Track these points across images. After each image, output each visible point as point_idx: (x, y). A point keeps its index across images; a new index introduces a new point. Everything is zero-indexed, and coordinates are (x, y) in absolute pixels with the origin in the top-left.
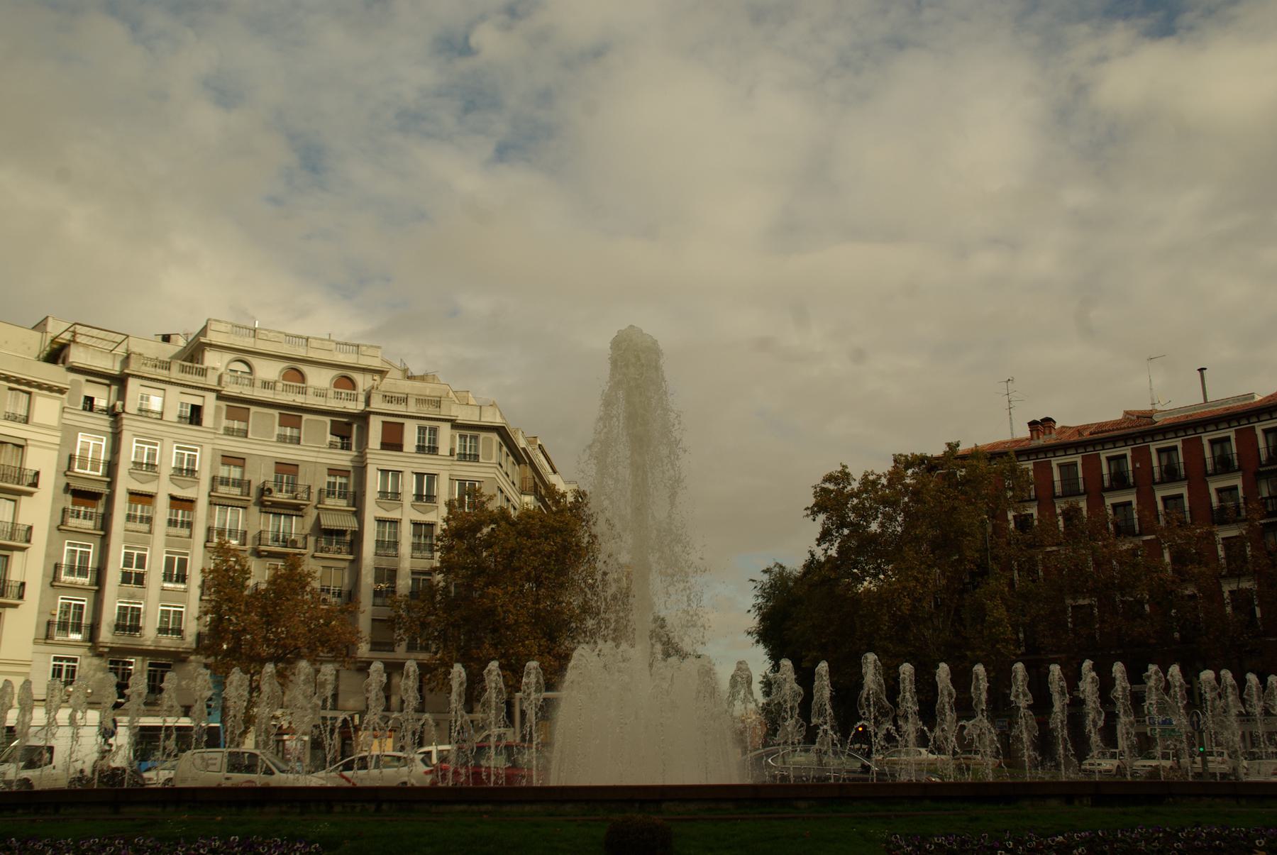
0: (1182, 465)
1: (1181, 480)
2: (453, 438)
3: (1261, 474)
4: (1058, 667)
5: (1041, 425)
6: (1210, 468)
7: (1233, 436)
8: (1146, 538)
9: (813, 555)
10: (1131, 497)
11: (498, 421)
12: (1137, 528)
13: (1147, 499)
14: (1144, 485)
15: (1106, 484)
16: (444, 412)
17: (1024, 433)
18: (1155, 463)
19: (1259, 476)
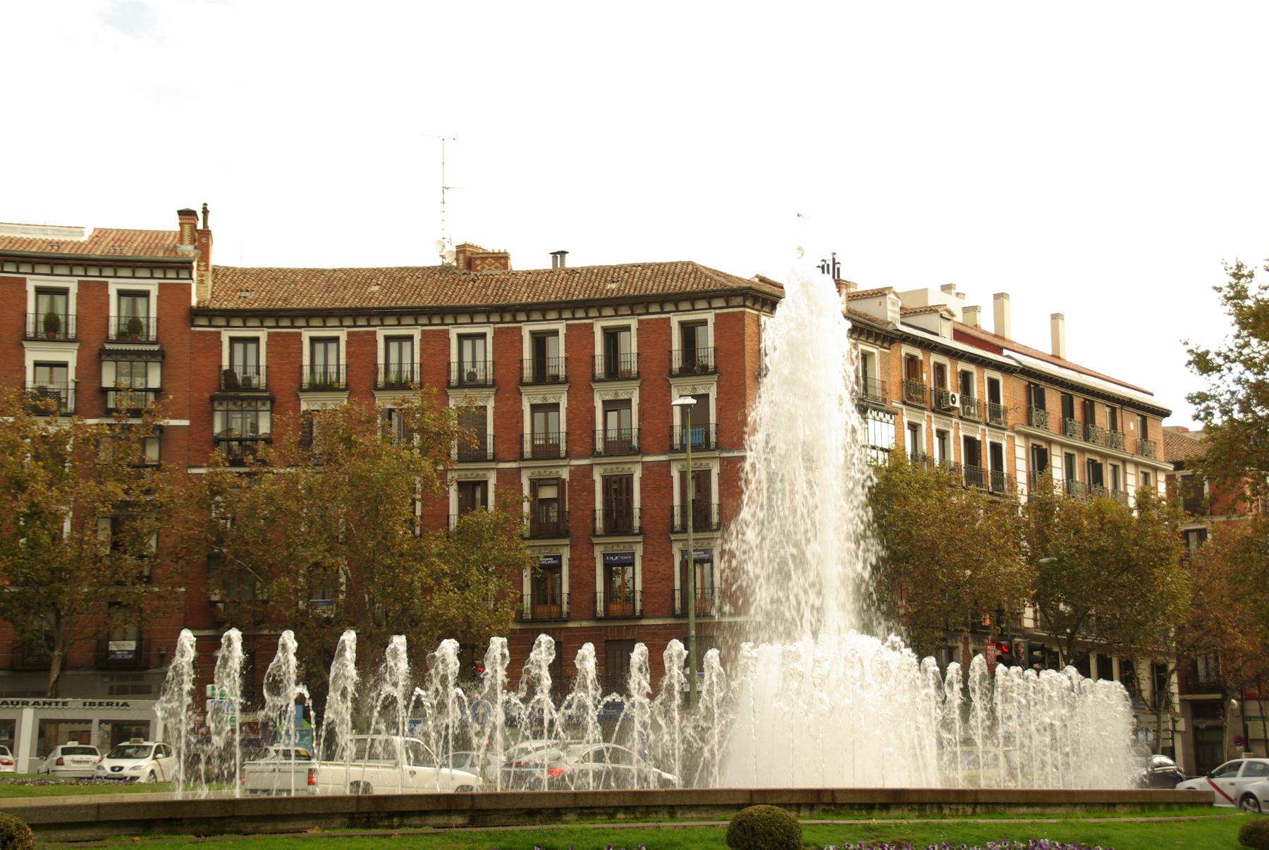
1: (67, 340)
3: (110, 353)
4: (292, 634)
5: (470, 258)
12: (563, 447)
18: (113, 311)
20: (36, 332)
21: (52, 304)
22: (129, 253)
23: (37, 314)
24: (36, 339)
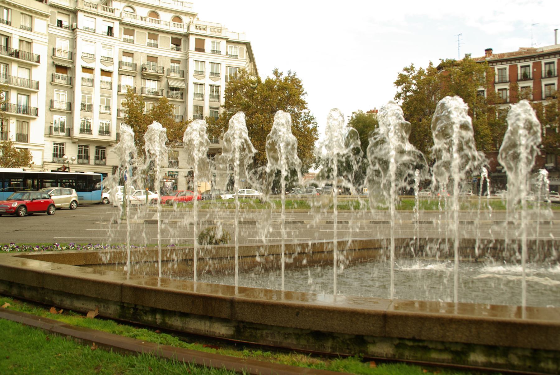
2: (227, 47)
8: (535, 102)
15: (519, 78)
16: (223, 35)
17: (483, 54)
18: (543, 69)
20: (545, 76)
21: (550, 67)
22: (505, 58)
23: (545, 70)
24: (545, 78)
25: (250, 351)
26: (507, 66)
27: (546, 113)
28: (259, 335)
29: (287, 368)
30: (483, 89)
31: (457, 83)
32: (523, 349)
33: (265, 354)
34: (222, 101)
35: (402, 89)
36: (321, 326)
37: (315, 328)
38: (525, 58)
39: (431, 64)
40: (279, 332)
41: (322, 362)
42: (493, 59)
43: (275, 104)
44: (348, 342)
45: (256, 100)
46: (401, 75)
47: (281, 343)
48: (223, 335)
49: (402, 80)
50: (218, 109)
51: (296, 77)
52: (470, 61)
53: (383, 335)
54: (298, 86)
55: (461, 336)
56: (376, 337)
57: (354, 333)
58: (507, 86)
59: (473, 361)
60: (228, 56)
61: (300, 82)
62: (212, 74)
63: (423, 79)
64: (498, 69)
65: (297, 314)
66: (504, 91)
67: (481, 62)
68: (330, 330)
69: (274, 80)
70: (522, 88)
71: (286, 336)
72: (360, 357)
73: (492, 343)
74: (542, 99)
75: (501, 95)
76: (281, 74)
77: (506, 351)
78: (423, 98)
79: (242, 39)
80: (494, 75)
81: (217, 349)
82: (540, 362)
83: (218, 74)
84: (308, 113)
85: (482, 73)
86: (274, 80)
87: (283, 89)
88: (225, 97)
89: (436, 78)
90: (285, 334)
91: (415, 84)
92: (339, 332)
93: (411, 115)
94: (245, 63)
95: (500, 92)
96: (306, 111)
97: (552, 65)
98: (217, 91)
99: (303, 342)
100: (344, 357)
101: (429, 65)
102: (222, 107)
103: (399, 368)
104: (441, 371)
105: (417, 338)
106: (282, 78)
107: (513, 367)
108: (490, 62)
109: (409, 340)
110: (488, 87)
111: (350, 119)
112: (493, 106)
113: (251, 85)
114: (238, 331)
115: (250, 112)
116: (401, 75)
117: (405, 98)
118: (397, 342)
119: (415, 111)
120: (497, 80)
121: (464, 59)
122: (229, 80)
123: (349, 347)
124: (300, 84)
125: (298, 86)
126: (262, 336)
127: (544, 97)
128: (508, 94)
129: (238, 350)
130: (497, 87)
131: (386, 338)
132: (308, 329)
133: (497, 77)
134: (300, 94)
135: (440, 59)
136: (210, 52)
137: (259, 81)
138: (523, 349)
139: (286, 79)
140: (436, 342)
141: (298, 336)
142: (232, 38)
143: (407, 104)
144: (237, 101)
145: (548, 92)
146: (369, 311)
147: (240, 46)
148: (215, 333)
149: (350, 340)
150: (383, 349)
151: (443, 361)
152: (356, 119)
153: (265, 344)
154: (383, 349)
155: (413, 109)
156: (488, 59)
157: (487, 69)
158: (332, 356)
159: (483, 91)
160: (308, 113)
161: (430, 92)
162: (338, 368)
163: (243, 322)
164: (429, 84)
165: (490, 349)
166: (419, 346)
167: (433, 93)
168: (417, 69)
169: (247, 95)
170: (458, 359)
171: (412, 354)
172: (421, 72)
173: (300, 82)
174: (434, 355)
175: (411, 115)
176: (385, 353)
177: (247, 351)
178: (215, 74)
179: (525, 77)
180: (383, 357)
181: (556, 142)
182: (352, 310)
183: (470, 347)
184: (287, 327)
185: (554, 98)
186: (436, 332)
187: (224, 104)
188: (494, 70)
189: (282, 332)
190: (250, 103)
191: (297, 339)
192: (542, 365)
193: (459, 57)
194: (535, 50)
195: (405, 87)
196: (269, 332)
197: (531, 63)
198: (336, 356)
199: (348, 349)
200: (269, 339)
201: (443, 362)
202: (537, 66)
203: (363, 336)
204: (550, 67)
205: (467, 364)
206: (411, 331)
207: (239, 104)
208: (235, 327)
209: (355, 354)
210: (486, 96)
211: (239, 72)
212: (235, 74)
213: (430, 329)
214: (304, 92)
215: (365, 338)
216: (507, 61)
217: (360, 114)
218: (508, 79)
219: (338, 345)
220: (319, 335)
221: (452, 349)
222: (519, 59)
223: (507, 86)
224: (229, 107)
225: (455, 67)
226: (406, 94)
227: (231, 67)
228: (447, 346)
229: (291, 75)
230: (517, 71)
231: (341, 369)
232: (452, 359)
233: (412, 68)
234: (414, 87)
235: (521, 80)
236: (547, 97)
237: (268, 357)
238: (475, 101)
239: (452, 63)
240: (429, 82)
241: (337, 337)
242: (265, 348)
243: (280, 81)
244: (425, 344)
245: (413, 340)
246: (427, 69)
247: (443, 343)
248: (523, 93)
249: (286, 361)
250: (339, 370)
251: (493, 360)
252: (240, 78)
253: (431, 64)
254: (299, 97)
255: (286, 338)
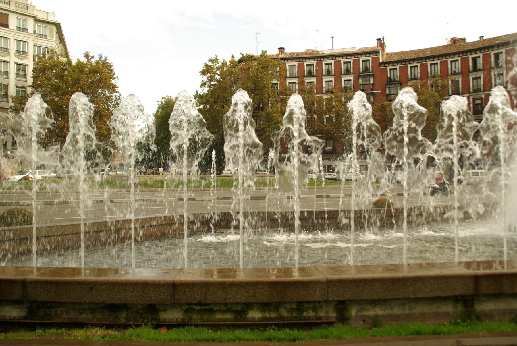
0: (371, 67)
1: (351, 74)
2: (34, 26)
6: (343, 72)
7: (315, 64)
8: (318, 95)
9: (197, 92)
10: (332, 79)
11: (56, 20)
13: (338, 80)
14: (319, 76)
15: (306, 74)
16: (30, 12)
17: (277, 52)
18: (361, 66)
19: (359, 76)
21: (347, 66)
22: (295, 56)
24: (344, 74)
25: (43, 331)
26: (296, 64)
27: (326, 105)
28: (53, 313)
29: (80, 342)
30: (277, 82)
31: (255, 75)
32: (291, 303)
33: (59, 331)
34: (30, 80)
35: (207, 78)
36: (115, 298)
37: (109, 301)
38: (310, 58)
39: (233, 57)
40: (74, 308)
41: (116, 333)
42: (285, 57)
43: (86, 86)
44: (141, 311)
45: (67, 81)
46: (206, 66)
47: (76, 318)
48: (14, 317)
49: (207, 70)
50: (25, 88)
51: (107, 61)
52: (266, 57)
53: (173, 302)
54: (109, 70)
55: (240, 297)
56: (167, 304)
57: (146, 302)
58: (295, 81)
59: (251, 318)
60: (36, 35)
61: (111, 66)
62: (18, 51)
63: (226, 70)
64: (289, 66)
65: (92, 289)
66: (294, 85)
67: (275, 59)
68: (123, 302)
69: (85, 62)
70: (308, 83)
71: (81, 311)
72: (152, 324)
73: (266, 301)
74: (323, 93)
75: (291, 88)
76: (92, 57)
77: (277, 306)
78: (225, 87)
79: (51, 19)
80: (286, 70)
81: (6, 333)
82: (303, 312)
83: (25, 53)
84: (119, 97)
85: (276, 68)
86: (85, 62)
87: (94, 72)
88: (33, 77)
89: (237, 70)
90: (80, 309)
91: (218, 75)
92: (132, 303)
93: (215, 102)
94: (54, 43)
95: (291, 85)
96: (117, 94)
97: (330, 66)
98: (24, 70)
99: (98, 316)
100: (138, 326)
101: (231, 58)
102: (30, 86)
103: (187, 331)
104: (224, 329)
105: (203, 302)
106: (93, 61)
107: (283, 318)
108: (282, 59)
109: (196, 304)
110: (280, 80)
111: (160, 103)
112: (285, 97)
113: (61, 66)
114: (31, 312)
115: (60, 93)
116: (206, 66)
117: (209, 87)
118: (186, 307)
119: (218, 98)
120: (288, 75)
121: (261, 55)
122: (37, 60)
123: (142, 316)
124: (112, 69)
125: (109, 70)
126: (56, 313)
127: (324, 91)
128: (297, 88)
129: (30, 331)
130: (288, 81)
131: (175, 305)
132: (103, 303)
133: (288, 72)
134: (111, 78)
135: (241, 54)
136: (15, 29)
137: (69, 63)
138: (291, 303)
139: (97, 63)
140: (220, 304)
141: (93, 311)
142: (40, 16)
143: (211, 92)
144: (46, 82)
145: (327, 88)
146: (159, 281)
147: (48, 26)
148: (5, 316)
149: (143, 309)
150: (174, 315)
151: (227, 320)
152: (165, 104)
153: (60, 321)
154: (174, 315)
155: (216, 97)
156: (281, 56)
157: (279, 65)
158: (126, 326)
159: (277, 84)
160: (119, 97)
161: (232, 82)
162: (131, 337)
163: (36, 302)
164: (231, 75)
165: (265, 306)
166: (205, 309)
167: (235, 84)
168: (221, 60)
169: (56, 76)
170: (239, 317)
171: (199, 317)
172: (224, 64)
173: (111, 66)
174: (219, 316)
175: (215, 102)
176: (175, 319)
177: (41, 331)
178: (22, 53)
179: (310, 74)
180: (174, 322)
181: (333, 129)
182: (145, 281)
183: (248, 306)
184: (81, 303)
185: (332, 93)
186: (219, 296)
187: (32, 84)
188: (286, 66)
189: (77, 308)
190: (60, 84)
191: (92, 313)
192: (305, 314)
193: (257, 53)
194: (318, 52)
195: (210, 77)
196: (63, 309)
197: (314, 63)
198: (130, 326)
199: (141, 318)
200: (64, 316)
201: (227, 321)
202: (319, 65)
203: (155, 305)
204: (347, 66)
205: (247, 321)
206: (197, 296)
207: (48, 84)
208: (27, 307)
209: (148, 322)
210: (279, 88)
211: (48, 52)
212: (44, 55)
213: (214, 293)
214: (115, 76)
215: (157, 306)
216: (296, 59)
217: (169, 100)
218: (297, 75)
219: (131, 315)
220: (113, 308)
221: (234, 309)
222: (306, 58)
223: (295, 81)
224: (38, 88)
225: (253, 62)
226: (210, 83)
227: (39, 47)
228: (229, 307)
229: (102, 59)
230: (341, 65)
231: (134, 338)
232: (234, 317)
233: (217, 60)
234: (218, 77)
235: (307, 76)
236: (327, 92)
237: (62, 334)
238: (270, 92)
239: (251, 58)
240: (231, 73)
241: (131, 308)
242: (60, 326)
243: (91, 64)
244: (211, 307)
245: (200, 304)
246: (230, 62)
247: (225, 304)
248: (308, 87)
249: (80, 336)
250: (132, 338)
251: (267, 315)
252: (49, 59)
253: (233, 57)
254: (110, 81)
255: (81, 313)
